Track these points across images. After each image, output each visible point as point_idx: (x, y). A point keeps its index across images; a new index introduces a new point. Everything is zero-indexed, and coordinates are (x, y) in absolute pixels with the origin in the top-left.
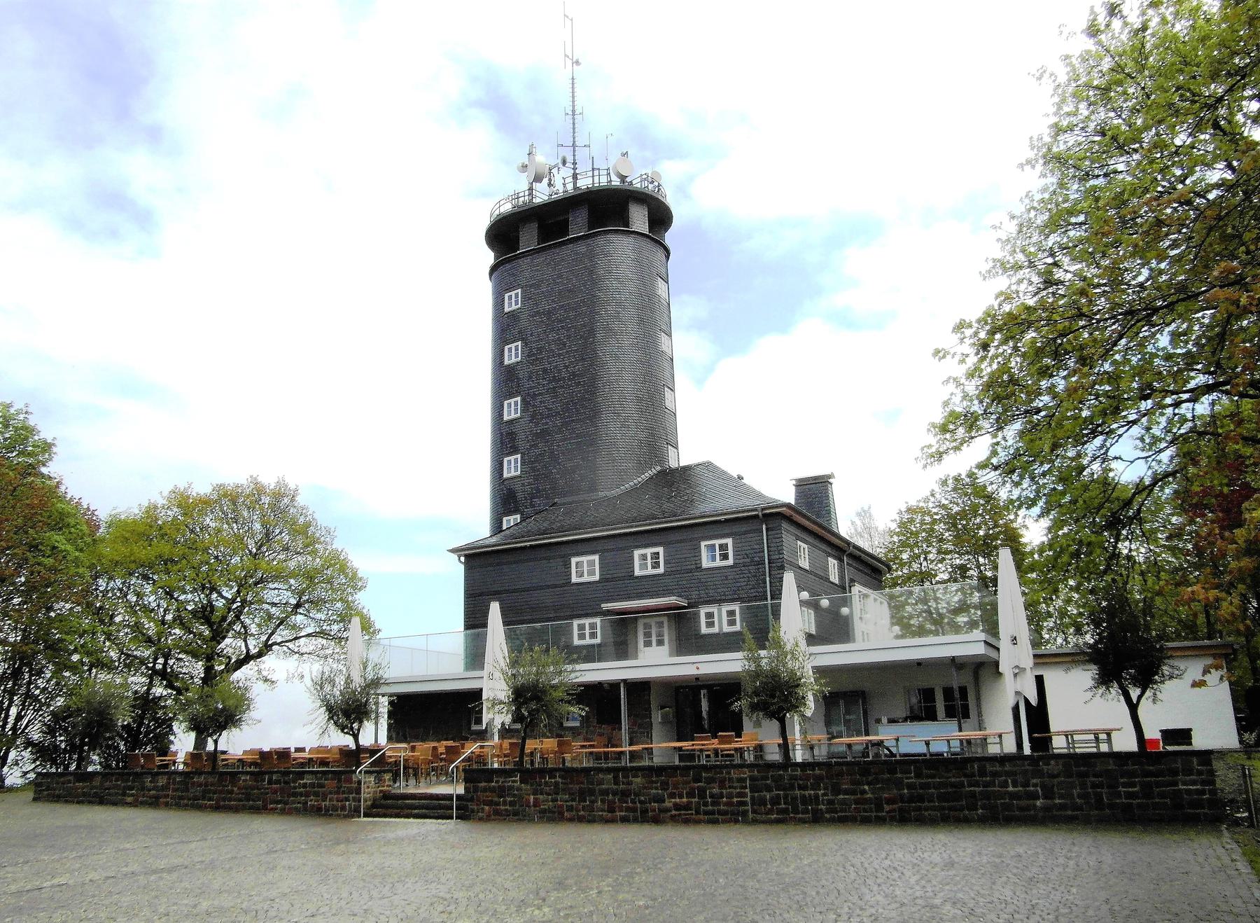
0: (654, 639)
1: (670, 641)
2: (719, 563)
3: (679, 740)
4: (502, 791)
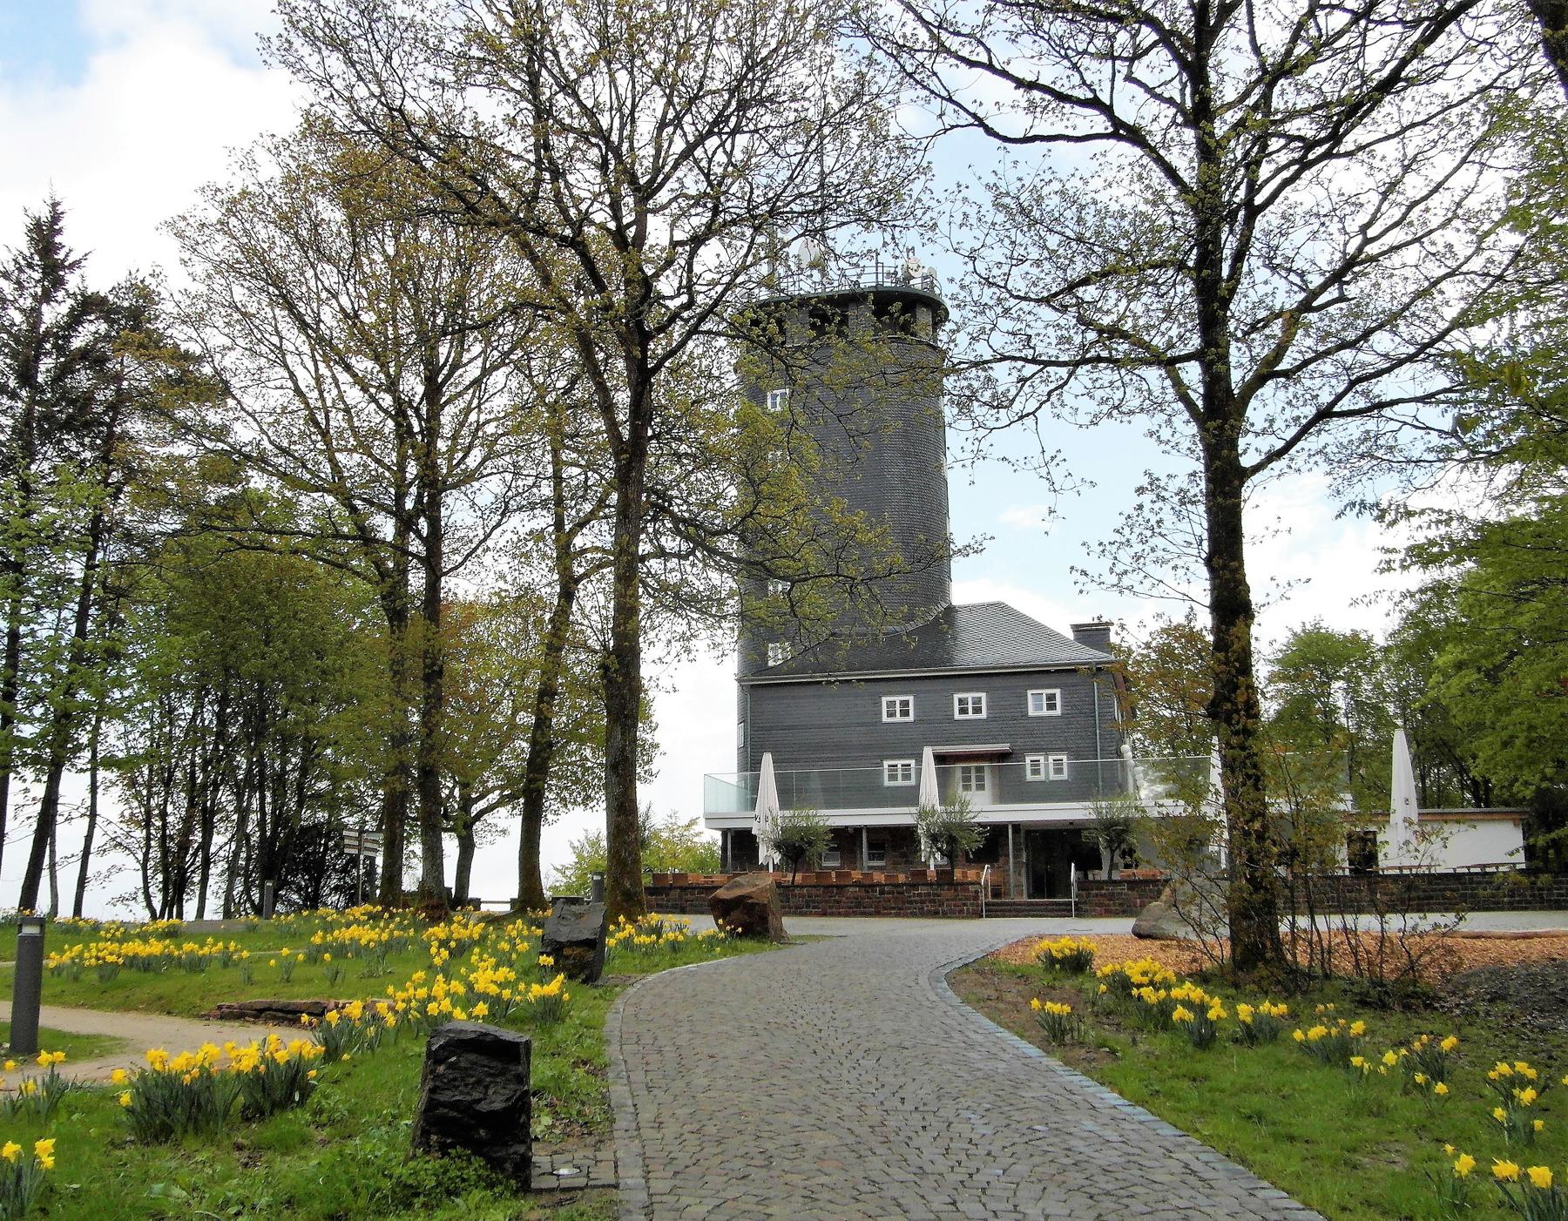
0: (973, 783)
1: (994, 785)
2: (1045, 712)
3: (1550, 830)
4: (1111, 897)
